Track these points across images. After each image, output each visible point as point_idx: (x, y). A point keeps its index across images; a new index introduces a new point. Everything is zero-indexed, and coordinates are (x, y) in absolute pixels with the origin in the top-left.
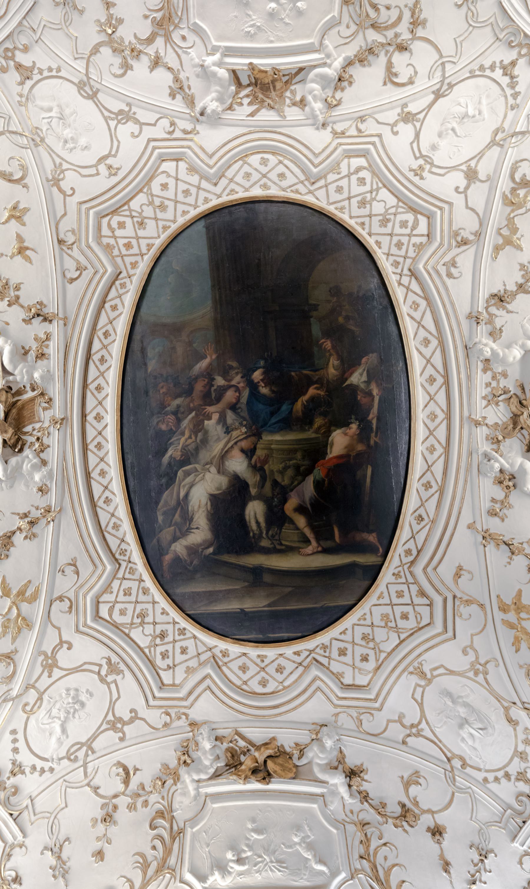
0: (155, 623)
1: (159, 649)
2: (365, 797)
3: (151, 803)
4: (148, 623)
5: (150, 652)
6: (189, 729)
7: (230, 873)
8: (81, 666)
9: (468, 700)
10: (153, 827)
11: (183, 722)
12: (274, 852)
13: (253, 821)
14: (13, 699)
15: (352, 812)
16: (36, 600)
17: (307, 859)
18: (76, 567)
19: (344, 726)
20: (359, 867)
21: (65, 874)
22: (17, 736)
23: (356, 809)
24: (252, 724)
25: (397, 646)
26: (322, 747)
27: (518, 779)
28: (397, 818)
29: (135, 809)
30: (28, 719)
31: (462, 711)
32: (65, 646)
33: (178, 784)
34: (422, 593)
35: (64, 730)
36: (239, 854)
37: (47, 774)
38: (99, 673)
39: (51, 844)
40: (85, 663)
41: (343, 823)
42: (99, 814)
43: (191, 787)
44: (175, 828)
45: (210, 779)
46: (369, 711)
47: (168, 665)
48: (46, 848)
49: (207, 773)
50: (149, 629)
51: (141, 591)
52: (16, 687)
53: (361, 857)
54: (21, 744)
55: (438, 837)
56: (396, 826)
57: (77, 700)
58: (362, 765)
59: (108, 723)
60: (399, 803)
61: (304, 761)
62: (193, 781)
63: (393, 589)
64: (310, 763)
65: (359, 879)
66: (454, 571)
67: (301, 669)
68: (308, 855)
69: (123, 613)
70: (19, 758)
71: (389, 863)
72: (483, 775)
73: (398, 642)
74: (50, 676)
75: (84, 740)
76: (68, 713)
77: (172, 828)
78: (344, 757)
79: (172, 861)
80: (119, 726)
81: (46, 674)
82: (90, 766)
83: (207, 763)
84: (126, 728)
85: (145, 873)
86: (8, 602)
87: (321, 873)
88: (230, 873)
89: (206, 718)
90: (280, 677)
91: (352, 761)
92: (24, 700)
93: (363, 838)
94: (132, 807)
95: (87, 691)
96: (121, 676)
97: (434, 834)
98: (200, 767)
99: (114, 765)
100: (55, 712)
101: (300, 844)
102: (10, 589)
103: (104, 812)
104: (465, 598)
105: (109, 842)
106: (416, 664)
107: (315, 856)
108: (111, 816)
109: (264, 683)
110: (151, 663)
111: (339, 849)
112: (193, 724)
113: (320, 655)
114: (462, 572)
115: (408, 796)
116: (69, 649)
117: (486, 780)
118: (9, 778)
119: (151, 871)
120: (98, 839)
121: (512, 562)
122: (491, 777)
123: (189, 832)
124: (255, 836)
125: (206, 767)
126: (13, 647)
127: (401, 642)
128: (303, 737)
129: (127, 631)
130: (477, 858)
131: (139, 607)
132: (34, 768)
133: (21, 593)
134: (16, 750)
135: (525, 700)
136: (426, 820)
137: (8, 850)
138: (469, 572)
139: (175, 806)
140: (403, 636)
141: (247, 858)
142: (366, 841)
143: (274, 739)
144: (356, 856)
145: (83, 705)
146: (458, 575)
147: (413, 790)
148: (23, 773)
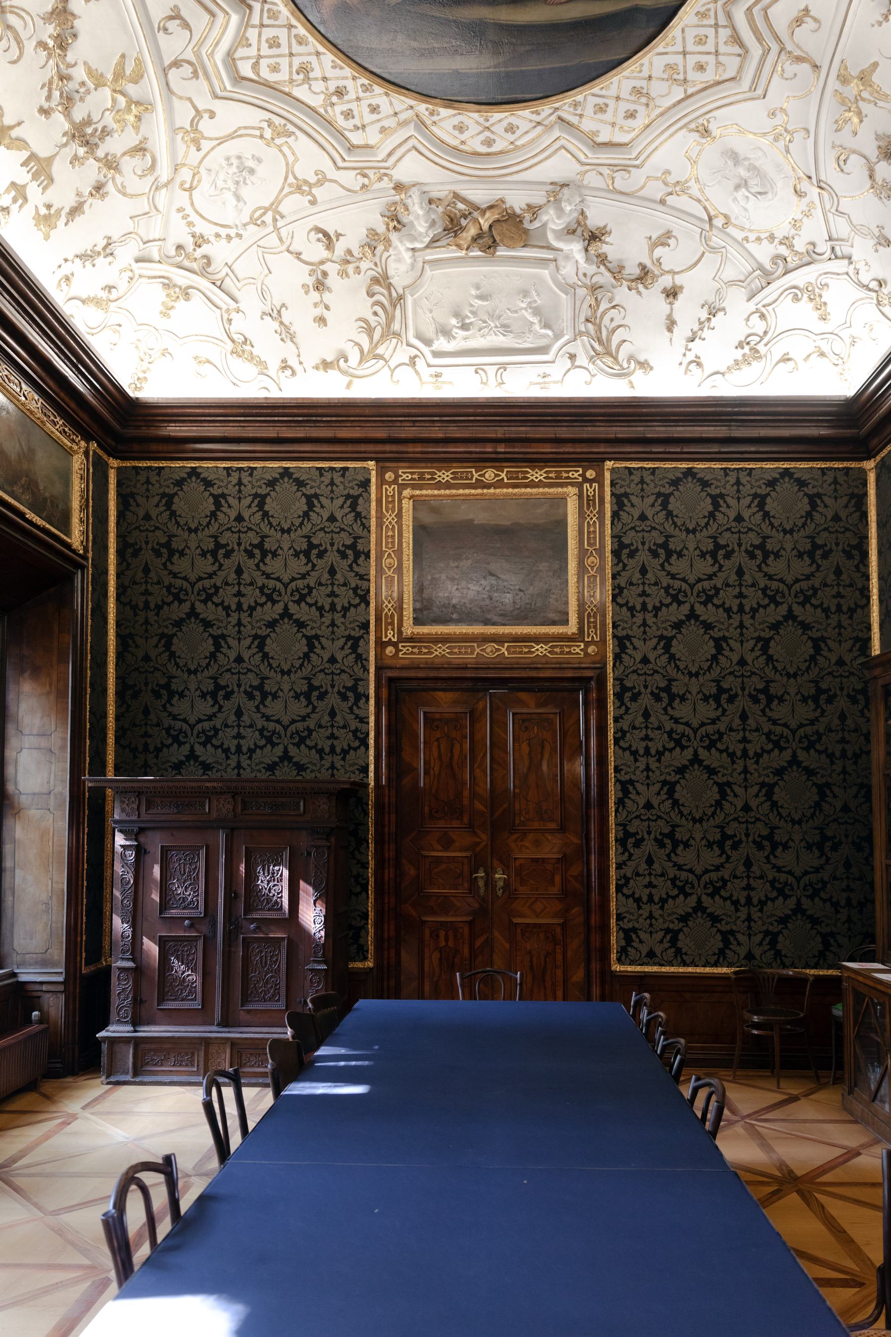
0: (325, 79)
1: (338, 109)
2: (602, 259)
3: (363, 270)
4: (316, 79)
5: (326, 111)
6: (393, 192)
7: (454, 338)
8: (236, 131)
9: (757, 164)
10: (371, 294)
11: (386, 183)
12: (499, 317)
13: (478, 287)
14: (166, 185)
15: (585, 275)
16: (142, 76)
17: (532, 323)
18: (181, 18)
19: (591, 185)
20: (583, 329)
21: (292, 338)
22: (186, 212)
23: (589, 274)
24: (474, 186)
25: (679, 102)
26: (560, 211)
27: (781, 243)
28: (633, 281)
29: (347, 275)
30: (191, 195)
31: (742, 172)
32: (206, 116)
33: (391, 250)
34: (736, 39)
35: (238, 198)
36: (463, 319)
37: (236, 240)
38: (262, 137)
39: (268, 309)
40: (240, 128)
41: (573, 287)
42: (311, 281)
43: (407, 256)
44: (394, 294)
45: (427, 247)
46: (625, 168)
47: (355, 126)
48: (264, 313)
49: (422, 242)
50: (319, 86)
51: (294, 41)
52: (164, 172)
53: (587, 320)
54: (194, 217)
55: (671, 299)
56: (630, 289)
57: (242, 169)
58: (605, 227)
59: (290, 185)
60: (640, 264)
61: (537, 224)
62: (408, 249)
63: (691, 34)
64: (544, 225)
65: (582, 341)
66: (795, 14)
67: (539, 129)
68: (535, 320)
69: (275, 69)
70: (198, 230)
71: (614, 324)
72: (743, 235)
73: (683, 96)
74: (199, 150)
75: (267, 205)
76: (237, 183)
77: (390, 295)
78: (586, 218)
79: (396, 326)
80: (305, 188)
81: (193, 149)
82: (284, 232)
83: (422, 230)
84: (314, 191)
85: (371, 338)
86: (107, 92)
87: (545, 336)
88: (454, 338)
89: (416, 180)
90: (511, 137)
91: (594, 221)
92: (178, 181)
93: (593, 303)
94: (343, 274)
95: (253, 156)
96: (293, 137)
97: (668, 296)
98: (413, 232)
99: (311, 230)
100: (220, 184)
101: (526, 309)
102: (102, 75)
103: (314, 278)
104: (797, 53)
105: (327, 308)
106: (700, 121)
107: (540, 321)
108: (323, 284)
109: (489, 143)
110: (329, 123)
111: (566, 313)
112: (399, 187)
113: (569, 112)
114: (807, 19)
115: (651, 257)
116: (211, 118)
117: (746, 239)
118: (194, 250)
119: (377, 335)
120: (316, 305)
121: (884, 24)
122: (752, 237)
123: (409, 300)
124: (480, 302)
125: (421, 234)
126: (140, 137)
127: (688, 97)
128: (538, 198)
129: (287, 90)
130: (704, 315)
131: (296, 62)
132: (218, 235)
133: (119, 75)
134: (190, 224)
135: (823, 178)
136: (666, 281)
137: (225, 316)
138: (816, 20)
139: (391, 272)
140: (690, 91)
141: (471, 323)
142: (594, 308)
143: (502, 201)
144: (582, 319)
145: (252, 171)
146: (799, 21)
147: (659, 251)
148: (208, 242)
